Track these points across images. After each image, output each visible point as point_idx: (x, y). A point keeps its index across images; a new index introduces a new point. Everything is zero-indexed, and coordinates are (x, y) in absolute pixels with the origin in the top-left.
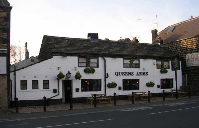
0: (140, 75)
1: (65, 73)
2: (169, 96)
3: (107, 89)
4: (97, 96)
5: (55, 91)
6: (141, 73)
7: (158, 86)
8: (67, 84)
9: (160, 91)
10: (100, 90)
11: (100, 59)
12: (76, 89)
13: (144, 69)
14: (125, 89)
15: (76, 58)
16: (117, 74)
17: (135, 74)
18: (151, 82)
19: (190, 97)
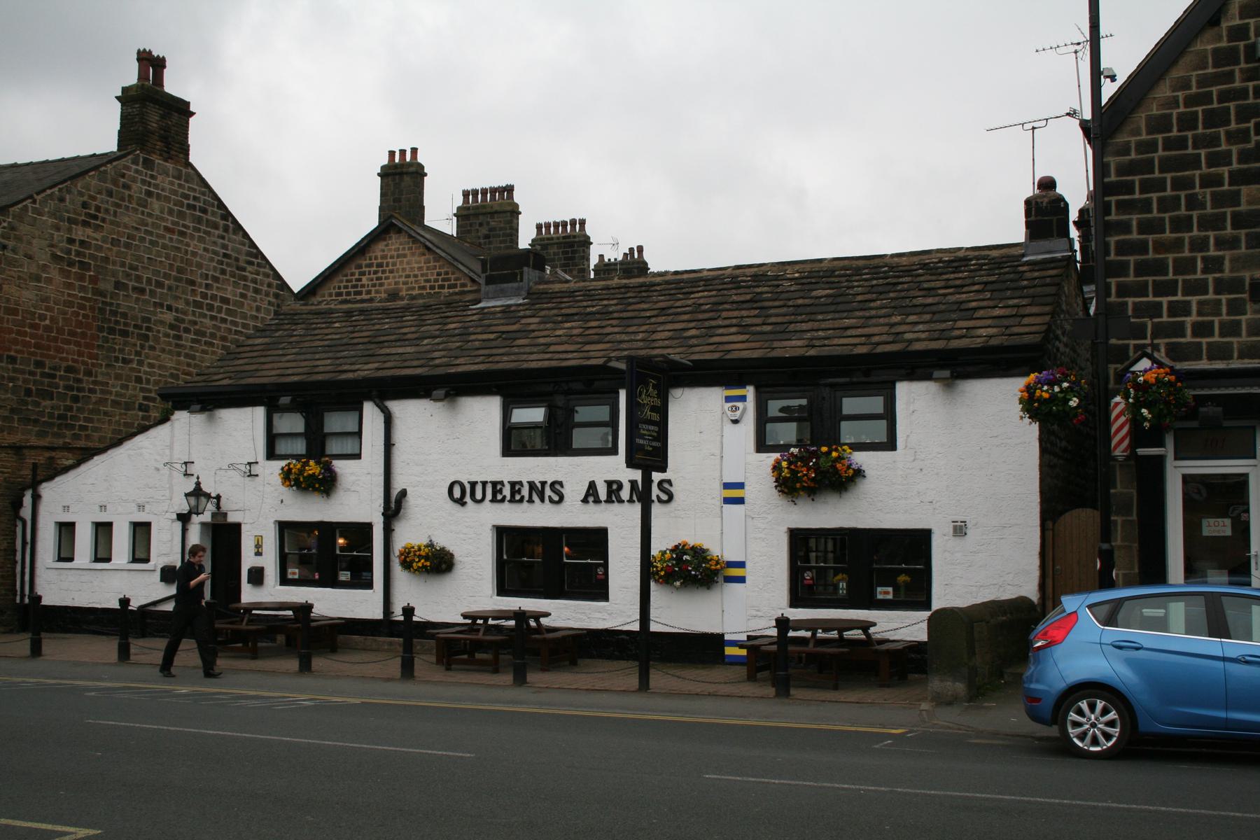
0: (609, 501)
4: (791, 634)
11: (371, 413)
16: (461, 494)
17: (574, 491)
18: (431, 545)
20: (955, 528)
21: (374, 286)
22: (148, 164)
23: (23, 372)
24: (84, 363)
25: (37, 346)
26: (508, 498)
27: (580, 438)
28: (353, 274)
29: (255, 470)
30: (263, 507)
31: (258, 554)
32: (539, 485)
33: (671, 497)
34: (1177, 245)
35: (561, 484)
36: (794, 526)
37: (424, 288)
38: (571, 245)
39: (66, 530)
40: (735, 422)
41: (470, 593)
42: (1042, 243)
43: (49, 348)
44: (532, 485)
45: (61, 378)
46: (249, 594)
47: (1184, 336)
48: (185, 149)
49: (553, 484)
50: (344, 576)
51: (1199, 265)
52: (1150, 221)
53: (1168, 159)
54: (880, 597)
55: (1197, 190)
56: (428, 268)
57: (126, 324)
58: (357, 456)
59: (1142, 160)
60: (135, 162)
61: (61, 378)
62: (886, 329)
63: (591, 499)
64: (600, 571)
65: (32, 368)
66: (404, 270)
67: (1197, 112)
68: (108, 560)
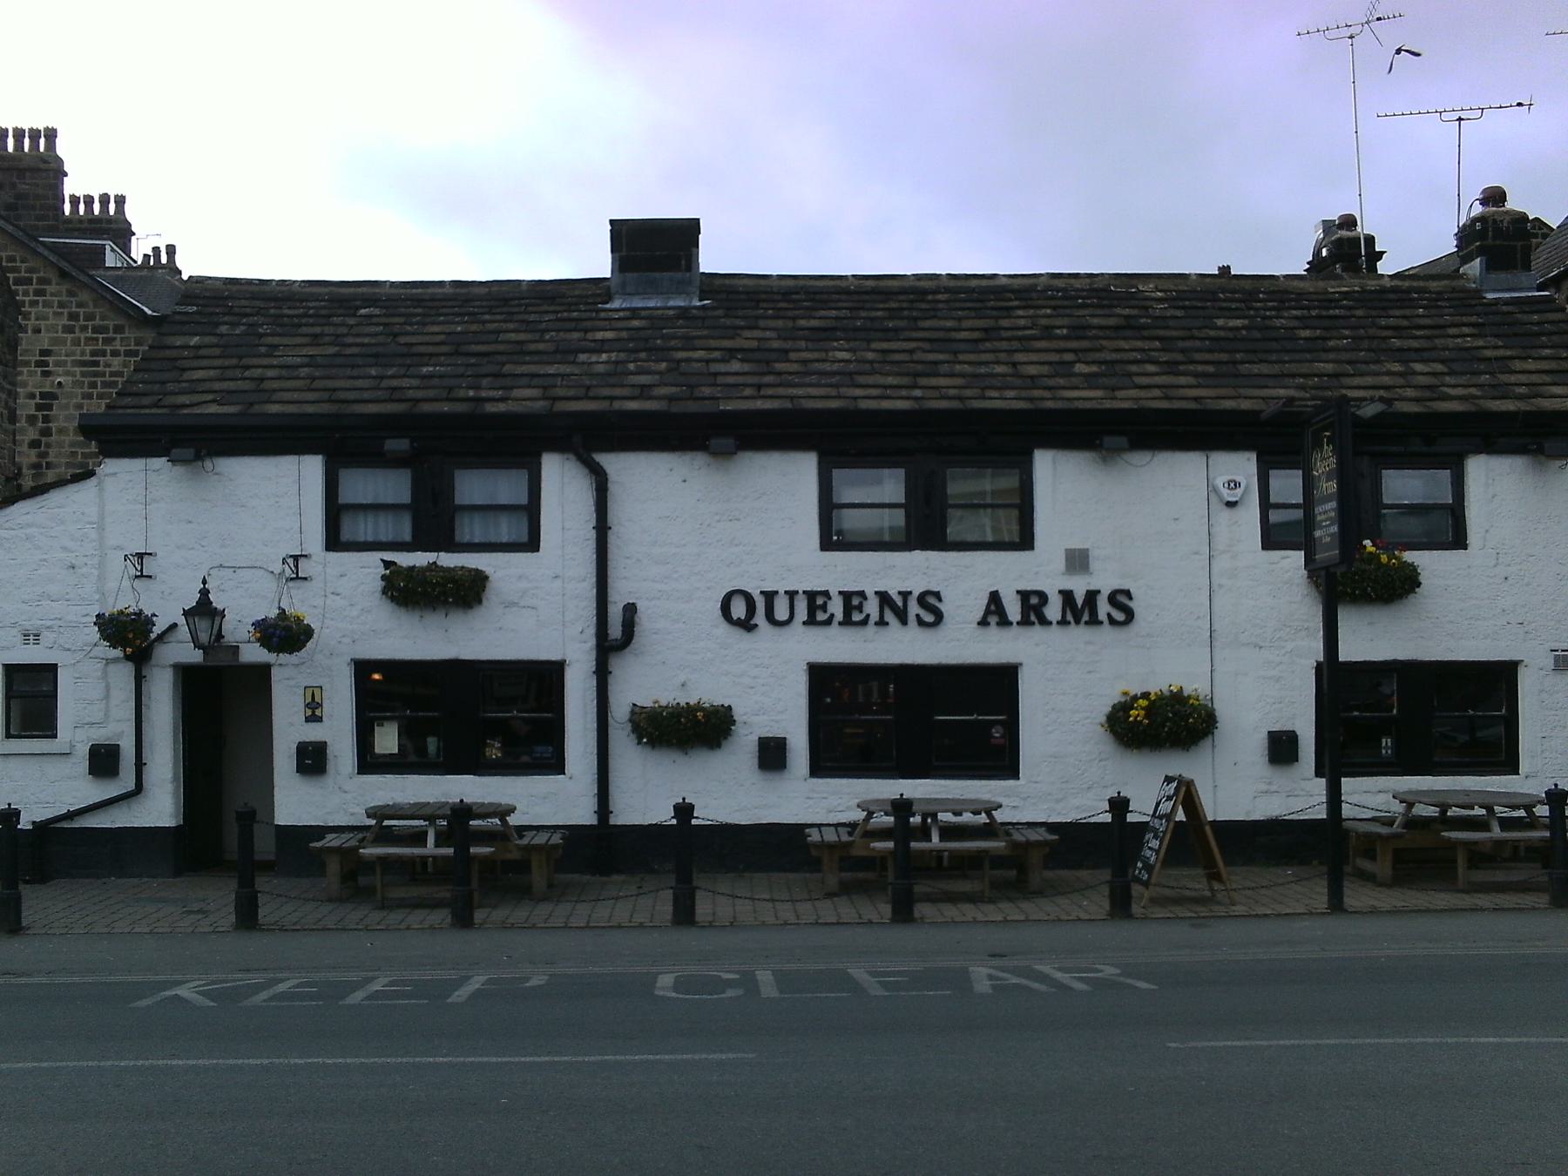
0: (1025, 622)
1: (166, 605)
2: (1480, 876)
5: (103, 761)
6: (1043, 597)
7: (1282, 748)
8: (221, 701)
9: (1299, 795)
10: (555, 764)
13: (1078, 561)
14: (830, 758)
15: (304, 476)
16: (745, 612)
17: (964, 604)
19: (903, 912)
26: (839, 616)
31: (313, 718)
32: (899, 601)
33: (1130, 615)
35: (937, 595)
42: (1503, 275)
44: (884, 597)
49: (922, 600)
50: (494, 752)
62: (326, 395)
63: (993, 620)
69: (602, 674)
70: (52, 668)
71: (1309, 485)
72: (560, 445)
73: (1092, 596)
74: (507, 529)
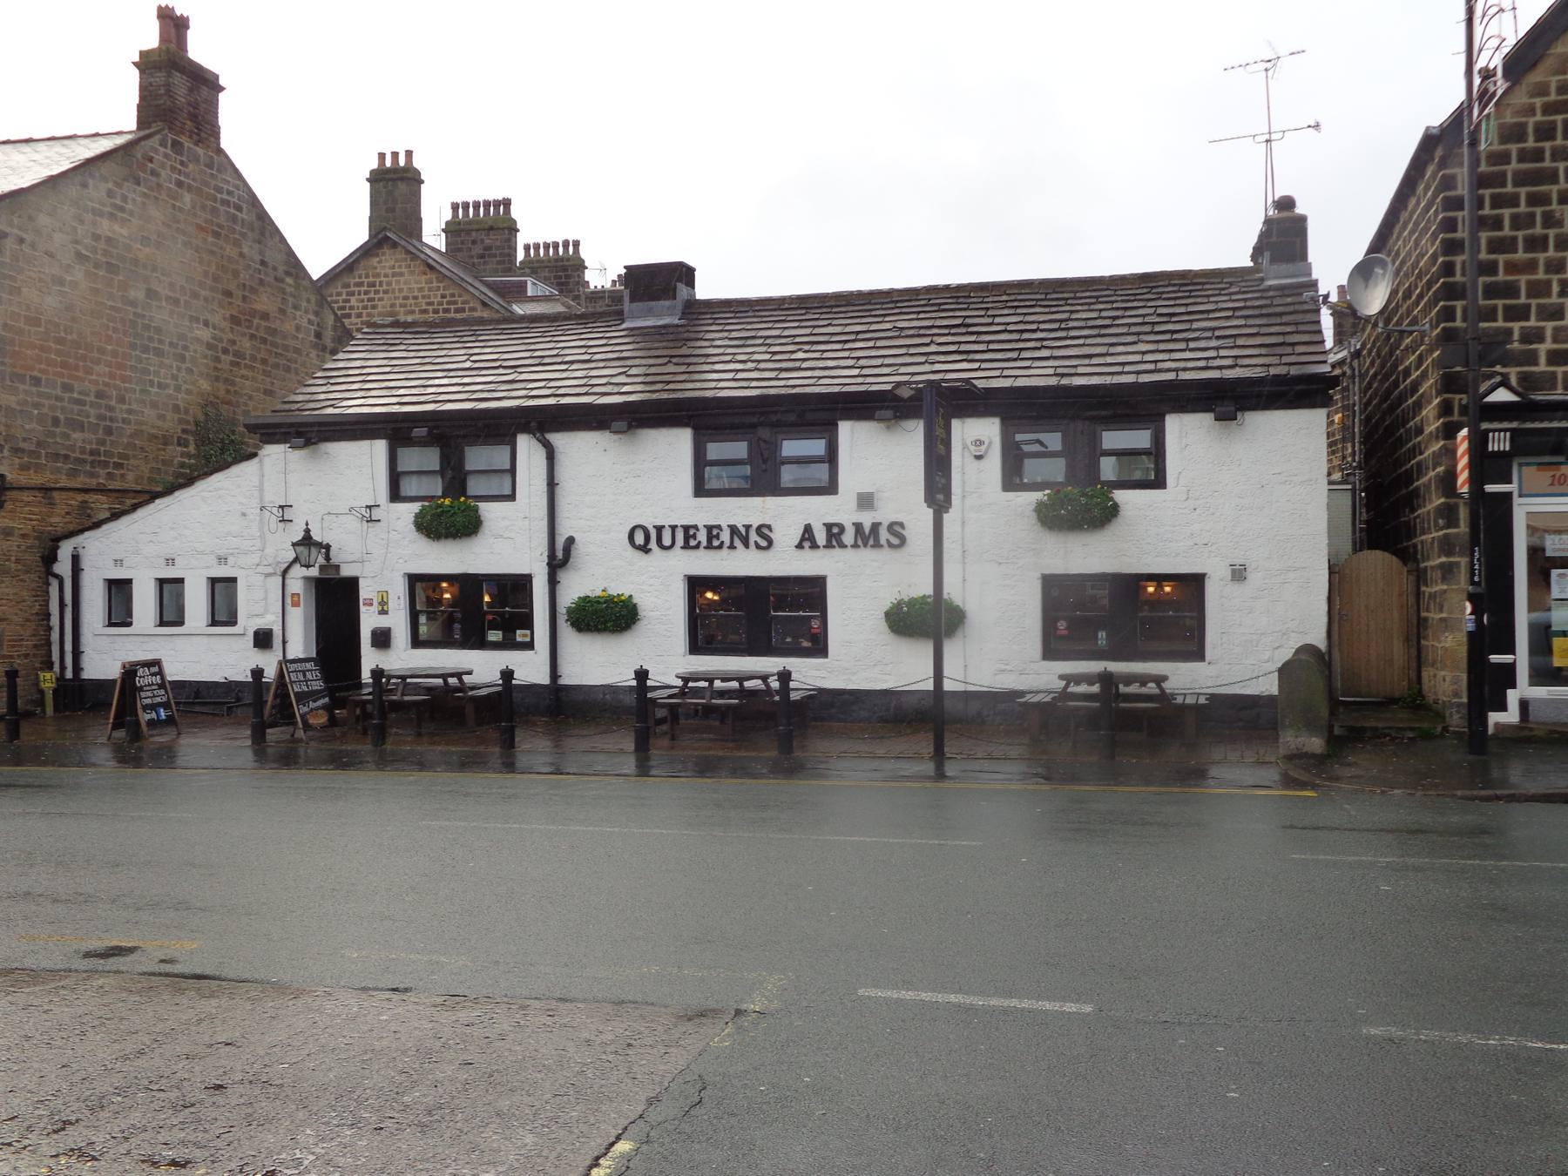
0: (829, 546)
3: (566, 633)
5: (263, 640)
6: (842, 529)
12: (389, 630)
16: (644, 540)
20: (1233, 571)
21: (365, 308)
22: (176, 145)
23: (49, 397)
24: (116, 387)
25: (64, 365)
26: (704, 543)
27: (788, 475)
28: (339, 294)
29: (376, 514)
30: (389, 556)
32: (743, 531)
33: (903, 541)
34: (1531, 266)
35: (769, 527)
36: (1047, 572)
37: (425, 311)
38: (565, 269)
39: (119, 590)
40: (979, 458)
41: (661, 653)
43: (76, 368)
44: (734, 530)
45: (92, 405)
46: (370, 659)
47: (1536, 364)
48: (215, 132)
49: (891, 527)
51: (1555, 288)
52: (1502, 240)
53: (1526, 173)
54: (519, 639)
55: (1554, 206)
56: (430, 289)
57: (160, 342)
58: (512, 497)
59: (1493, 173)
60: (163, 144)
61: (92, 405)
63: (807, 544)
64: (815, 624)
65: (59, 392)
66: (401, 290)
67: (1554, 122)
68: (180, 623)
69: (553, 582)
70: (234, 580)
71: (1494, 431)
72: (526, 429)
73: (875, 527)
74: (1144, 469)
